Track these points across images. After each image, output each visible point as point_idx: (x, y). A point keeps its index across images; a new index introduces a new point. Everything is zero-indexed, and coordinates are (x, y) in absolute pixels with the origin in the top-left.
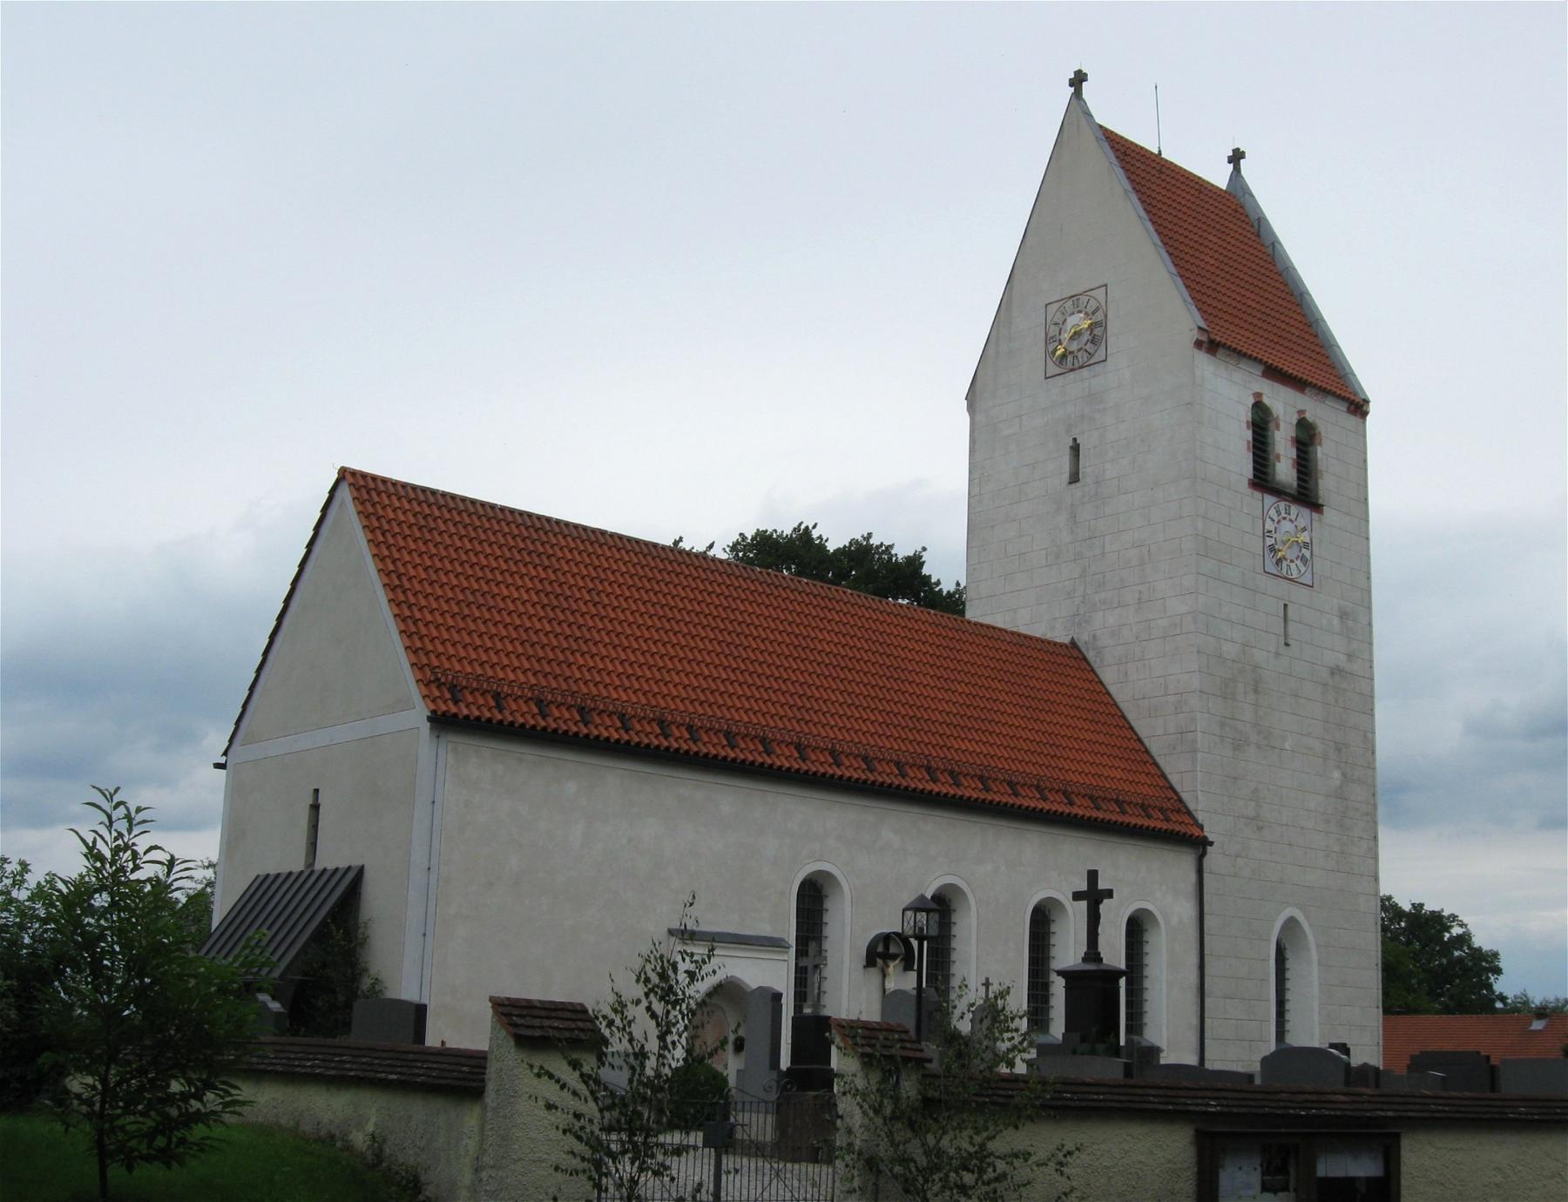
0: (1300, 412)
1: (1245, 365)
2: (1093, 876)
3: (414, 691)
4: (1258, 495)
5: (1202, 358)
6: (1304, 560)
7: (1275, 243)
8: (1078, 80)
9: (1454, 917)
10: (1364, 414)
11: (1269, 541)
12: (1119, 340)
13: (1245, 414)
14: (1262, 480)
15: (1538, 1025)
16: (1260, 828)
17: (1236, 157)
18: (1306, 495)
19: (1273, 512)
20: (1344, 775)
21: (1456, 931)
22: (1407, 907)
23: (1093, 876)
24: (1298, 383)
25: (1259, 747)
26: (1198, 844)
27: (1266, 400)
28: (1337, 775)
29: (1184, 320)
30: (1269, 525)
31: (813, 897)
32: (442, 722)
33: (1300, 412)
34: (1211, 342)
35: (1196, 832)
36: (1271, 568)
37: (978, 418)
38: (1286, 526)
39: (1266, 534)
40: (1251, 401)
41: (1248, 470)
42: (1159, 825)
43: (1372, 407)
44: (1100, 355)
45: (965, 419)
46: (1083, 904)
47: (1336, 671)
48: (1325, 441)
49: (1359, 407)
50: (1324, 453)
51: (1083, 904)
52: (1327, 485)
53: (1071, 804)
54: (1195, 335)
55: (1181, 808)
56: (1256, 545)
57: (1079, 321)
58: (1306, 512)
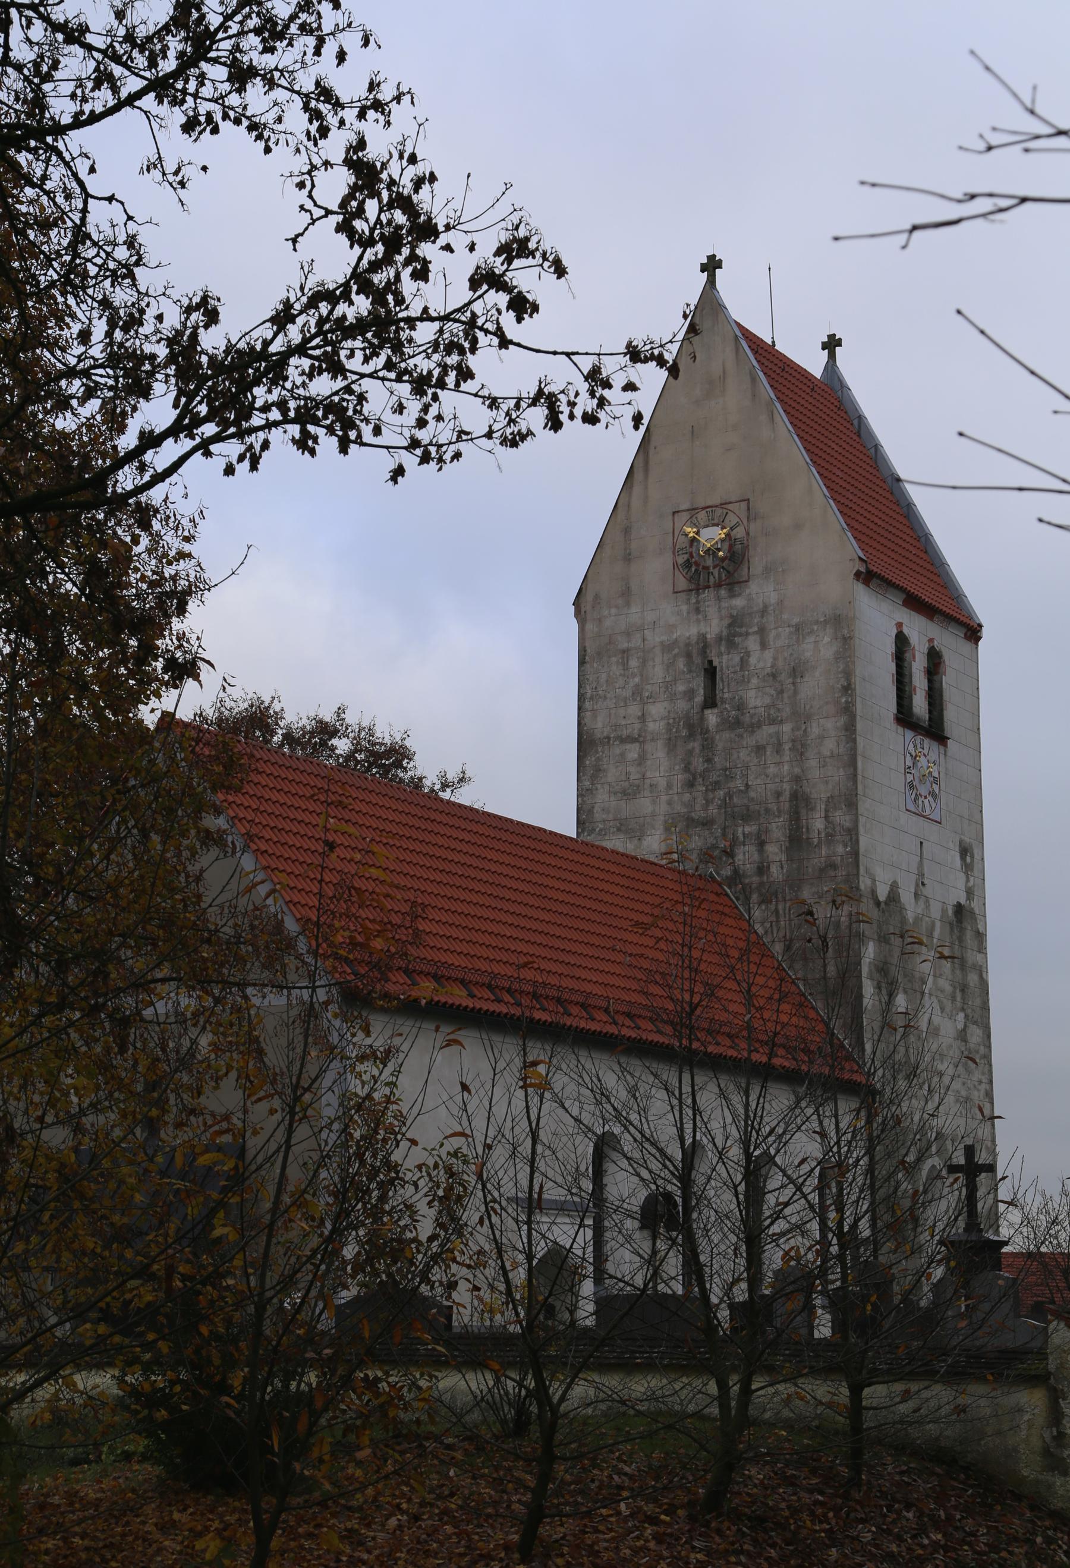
0: (931, 640)
4: (900, 729)
5: (860, 588)
7: (877, 447)
8: (711, 265)
11: (910, 778)
13: (890, 648)
14: (904, 718)
17: (832, 344)
18: (935, 731)
20: (966, 1016)
27: (906, 630)
33: (931, 640)
37: (589, 626)
40: (894, 632)
41: (893, 708)
43: (985, 632)
48: (948, 670)
49: (973, 633)
50: (948, 680)
52: (951, 714)
56: (898, 781)
57: (712, 536)
58: (935, 745)
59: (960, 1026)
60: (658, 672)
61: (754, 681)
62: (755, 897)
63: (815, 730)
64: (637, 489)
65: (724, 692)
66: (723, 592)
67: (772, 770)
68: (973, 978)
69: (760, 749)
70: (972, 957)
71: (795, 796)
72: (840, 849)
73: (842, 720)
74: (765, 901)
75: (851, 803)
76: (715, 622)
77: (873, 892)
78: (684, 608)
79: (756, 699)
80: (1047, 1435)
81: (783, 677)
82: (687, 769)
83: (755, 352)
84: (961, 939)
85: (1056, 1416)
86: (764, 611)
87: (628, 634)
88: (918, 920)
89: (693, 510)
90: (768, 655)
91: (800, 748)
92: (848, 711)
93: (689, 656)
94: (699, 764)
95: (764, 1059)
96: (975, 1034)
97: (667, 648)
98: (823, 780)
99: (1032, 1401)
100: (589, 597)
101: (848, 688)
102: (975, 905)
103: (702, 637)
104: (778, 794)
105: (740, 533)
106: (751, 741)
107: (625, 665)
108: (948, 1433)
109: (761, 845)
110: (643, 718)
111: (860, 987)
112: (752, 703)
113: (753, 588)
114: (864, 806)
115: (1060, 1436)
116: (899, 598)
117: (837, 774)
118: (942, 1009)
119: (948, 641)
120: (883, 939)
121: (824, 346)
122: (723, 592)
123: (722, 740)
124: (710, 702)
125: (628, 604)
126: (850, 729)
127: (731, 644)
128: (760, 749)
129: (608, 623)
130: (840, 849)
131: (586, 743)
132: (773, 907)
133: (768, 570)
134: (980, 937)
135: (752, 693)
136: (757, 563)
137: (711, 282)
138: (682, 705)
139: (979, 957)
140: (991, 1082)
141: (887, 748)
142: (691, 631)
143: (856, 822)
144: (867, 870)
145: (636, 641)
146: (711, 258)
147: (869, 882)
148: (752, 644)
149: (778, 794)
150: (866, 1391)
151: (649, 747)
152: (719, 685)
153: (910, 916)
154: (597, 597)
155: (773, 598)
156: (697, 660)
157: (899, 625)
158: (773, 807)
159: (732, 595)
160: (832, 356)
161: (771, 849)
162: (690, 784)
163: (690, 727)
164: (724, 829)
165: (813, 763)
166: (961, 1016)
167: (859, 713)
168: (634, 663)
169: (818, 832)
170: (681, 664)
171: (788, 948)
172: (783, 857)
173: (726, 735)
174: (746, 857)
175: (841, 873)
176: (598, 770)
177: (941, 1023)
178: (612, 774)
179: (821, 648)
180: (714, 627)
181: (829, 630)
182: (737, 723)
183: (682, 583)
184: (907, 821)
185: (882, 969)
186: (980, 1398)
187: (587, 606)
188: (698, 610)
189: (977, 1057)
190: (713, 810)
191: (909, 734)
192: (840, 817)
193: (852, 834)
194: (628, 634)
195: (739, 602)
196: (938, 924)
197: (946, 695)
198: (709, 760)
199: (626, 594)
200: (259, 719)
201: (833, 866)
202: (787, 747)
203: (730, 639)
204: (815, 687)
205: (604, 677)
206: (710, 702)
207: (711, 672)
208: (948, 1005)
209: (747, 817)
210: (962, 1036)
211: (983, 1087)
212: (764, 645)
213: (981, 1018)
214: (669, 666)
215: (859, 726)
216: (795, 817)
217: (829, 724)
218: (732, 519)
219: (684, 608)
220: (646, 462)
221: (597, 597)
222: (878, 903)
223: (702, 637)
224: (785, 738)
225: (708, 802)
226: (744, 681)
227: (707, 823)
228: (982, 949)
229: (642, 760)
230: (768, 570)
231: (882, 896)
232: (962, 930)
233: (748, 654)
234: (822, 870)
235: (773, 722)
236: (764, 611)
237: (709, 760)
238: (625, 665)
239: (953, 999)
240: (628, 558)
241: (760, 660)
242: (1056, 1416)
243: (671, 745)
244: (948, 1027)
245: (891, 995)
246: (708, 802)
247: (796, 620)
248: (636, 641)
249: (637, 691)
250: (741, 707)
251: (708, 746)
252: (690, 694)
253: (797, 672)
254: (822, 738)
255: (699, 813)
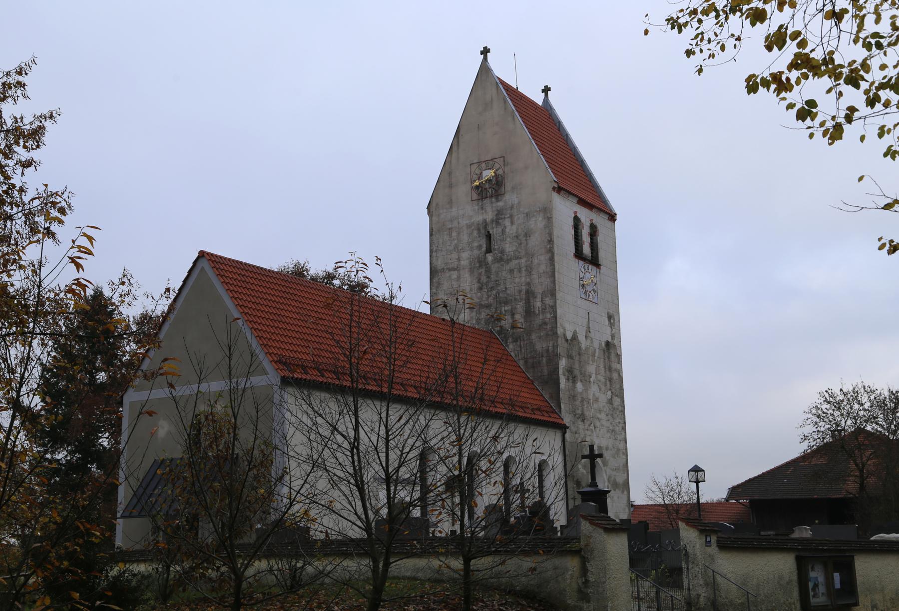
1: (571, 198)
5: (555, 195)
6: (594, 291)
7: (567, 135)
8: (485, 51)
10: (615, 220)
14: (579, 255)
17: (546, 90)
18: (594, 261)
24: (589, 206)
27: (579, 215)
30: (582, 275)
34: (559, 187)
35: (560, 421)
36: (583, 296)
37: (434, 218)
38: (588, 275)
39: (581, 279)
42: (547, 419)
43: (618, 217)
45: (427, 218)
49: (612, 217)
50: (600, 239)
52: (602, 255)
53: (406, 390)
56: (577, 285)
57: (489, 174)
59: (609, 397)
60: (465, 238)
61: (508, 240)
62: (510, 339)
63: (536, 261)
64: (454, 155)
65: (495, 246)
66: (493, 200)
67: (517, 280)
68: (615, 376)
69: (511, 271)
70: (614, 366)
71: (527, 292)
72: (548, 316)
73: (548, 256)
74: (515, 340)
75: (553, 293)
76: (490, 213)
77: (565, 335)
78: (476, 207)
79: (509, 248)
80: (580, 582)
81: (521, 237)
82: (479, 282)
83: (507, 90)
84: (609, 358)
85: (584, 571)
86: (512, 207)
87: (451, 221)
88: (587, 348)
89: (479, 163)
90: (514, 227)
91: (529, 270)
92: (551, 251)
93: (479, 230)
94: (484, 279)
95: (439, 399)
96: (617, 401)
97: (469, 226)
98: (540, 284)
99: (572, 564)
100: (434, 205)
101: (551, 241)
102: (616, 342)
103: (485, 221)
104: (520, 291)
105: (500, 172)
106: (507, 267)
107: (450, 235)
108: (532, 582)
109: (513, 315)
110: (459, 259)
111: (558, 379)
112: (507, 250)
113: (507, 197)
114: (559, 295)
115: (586, 582)
116: (575, 200)
117: (546, 281)
118: (600, 389)
119: (600, 221)
120: (570, 357)
121: (482, 53)
122: (493, 200)
123: (494, 267)
124: (489, 250)
125: (451, 208)
126: (552, 260)
127: (498, 223)
128: (511, 271)
129: (442, 216)
130: (548, 316)
131: (433, 272)
132: (518, 343)
133: (513, 188)
134: (619, 357)
135: (507, 246)
136: (508, 185)
137: (485, 59)
138: (476, 252)
139: (618, 366)
140: (625, 423)
141: (570, 270)
142: (479, 218)
143: (555, 302)
144: (561, 325)
145: (455, 224)
146: (485, 48)
147: (562, 330)
148: (507, 222)
149: (520, 291)
150: (473, 562)
151: (462, 272)
152: (493, 242)
153: (583, 346)
154: (437, 204)
155: (516, 201)
156: (483, 231)
157: (575, 213)
158: (518, 297)
159: (498, 201)
160: (546, 95)
161: (517, 317)
162: (481, 289)
163: (480, 262)
164: (496, 309)
165: (535, 276)
166: (609, 393)
167: (556, 252)
168: (454, 234)
169: (539, 310)
170: (475, 233)
171: (526, 362)
172: (523, 320)
173: (497, 265)
174: (506, 323)
175: (549, 326)
176: (439, 284)
177: (596, 392)
178: (446, 285)
179: (538, 223)
180: (489, 216)
181: (542, 214)
182: (501, 259)
183: (475, 196)
184: (580, 302)
185: (570, 371)
186: (548, 564)
187: (433, 209)
188: (482, 208)
189: (617, 409)
190: (491, 300)
191: (581, 263)
192: (549, 301)
193: (554, 308)
194: (451, 221)
195: (500, 204)
196: (597, 350)
197: (599, 246)
198: (488, 277)
199: (450, 202)
200: (299, 272)
201: (545, 323)
202: (523, 269)
203: (497, 221)
204: (536, 241)
205: (441, 241)
206: (489, 250)
207: (489, 236)
208: (603, 387)
209: (506, 303)
210: (610, 402)
211: (621, 425)
212: (512, 223)
213: (619, 393)
214: (470, 234)
215: (556, 258)
216: (528, 301)
217: (542, 258)
218: (497, 166)
219: (476, 207)
220: (458, 142)
221: (437, 204)
222: (567, 340)
223: (485, 221)
224: (523, 265)
225: (489, 296)
226: (503, 240)
227: (488, 306)
228: (619, 361)
229: (459, 278)
230: (513, 188)
231: (569, 336)
232: (609, 353)
233: (505, 227)
234: (540, 326)
235: (518, 258)
236: (512, 207)
237: (488, 277)
238: (450, 235)
239: (606, 385)
240: (451, 186)
241: (511, 230)
242: (584, 571)
243: (471, 271)
244: (603, 398)
245: (574, 382)
246: (489, 296)
247: (526, 211)
248: (455, 224)
249: (456, 247)
250: (502, 252)
251: (488, 271)
252: (480, 247)
253: (527, 235)
254: (539, 264)
255: (484, 302)
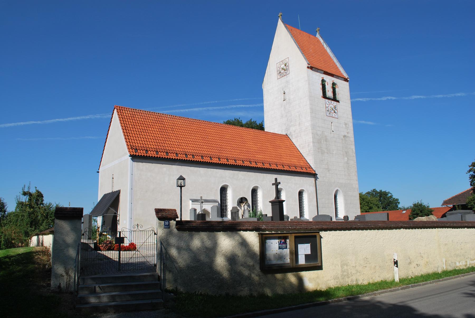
2: (276, 179)
3: (127, 150)
9: (389, 193)
11: (327, 109)
12: (291, 68)
14: (325, 96)
15: (404, 212)
16: (329, 171)
18: (335, 99)
19: (328, 103)
21: (389, 195)
22: (378, 191)
23: (276, 179)
24: (332, 75)
25: (327, 153)
26: (314, 175)
28: (346, 158)
29: (304, 63)
30: (327, 106)
31: (223, 190)
32: (135, 158)
35: (314, 172)
39: (326, 107)
41: (321, 94)
44: (288, 73)
46: (274, 186)
47: (345, 136)
51: (274, 186)
54: (307, 65)
55: (310, 167)
56: (324, 110)
